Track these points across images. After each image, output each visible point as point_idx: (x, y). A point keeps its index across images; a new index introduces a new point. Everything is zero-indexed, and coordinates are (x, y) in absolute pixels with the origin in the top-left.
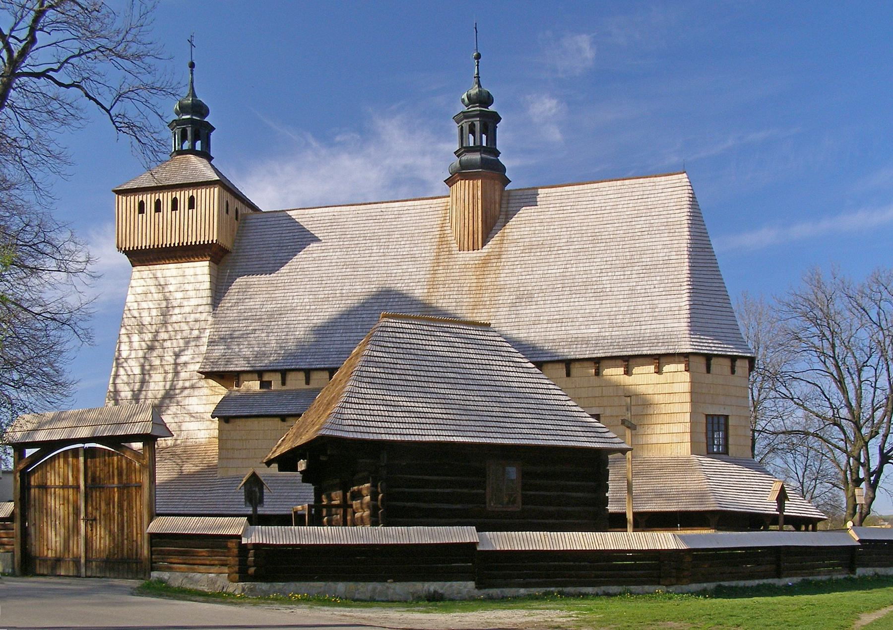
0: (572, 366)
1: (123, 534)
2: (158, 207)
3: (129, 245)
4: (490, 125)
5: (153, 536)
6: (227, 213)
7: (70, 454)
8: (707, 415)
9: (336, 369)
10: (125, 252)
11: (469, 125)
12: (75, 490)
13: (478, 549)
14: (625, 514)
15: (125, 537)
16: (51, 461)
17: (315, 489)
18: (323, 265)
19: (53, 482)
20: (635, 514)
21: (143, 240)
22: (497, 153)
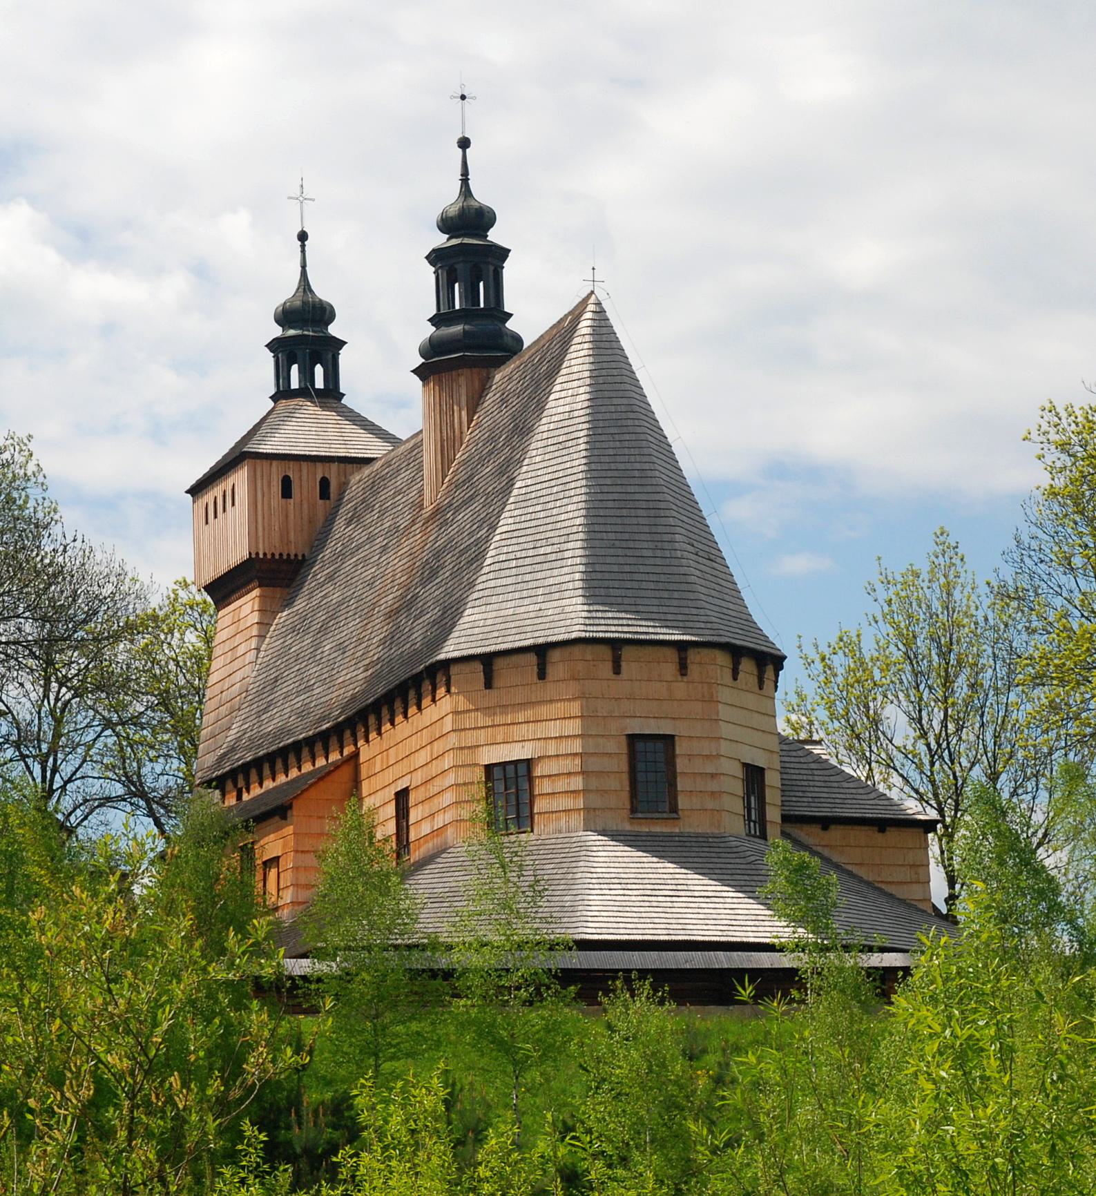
6: (207, 523)
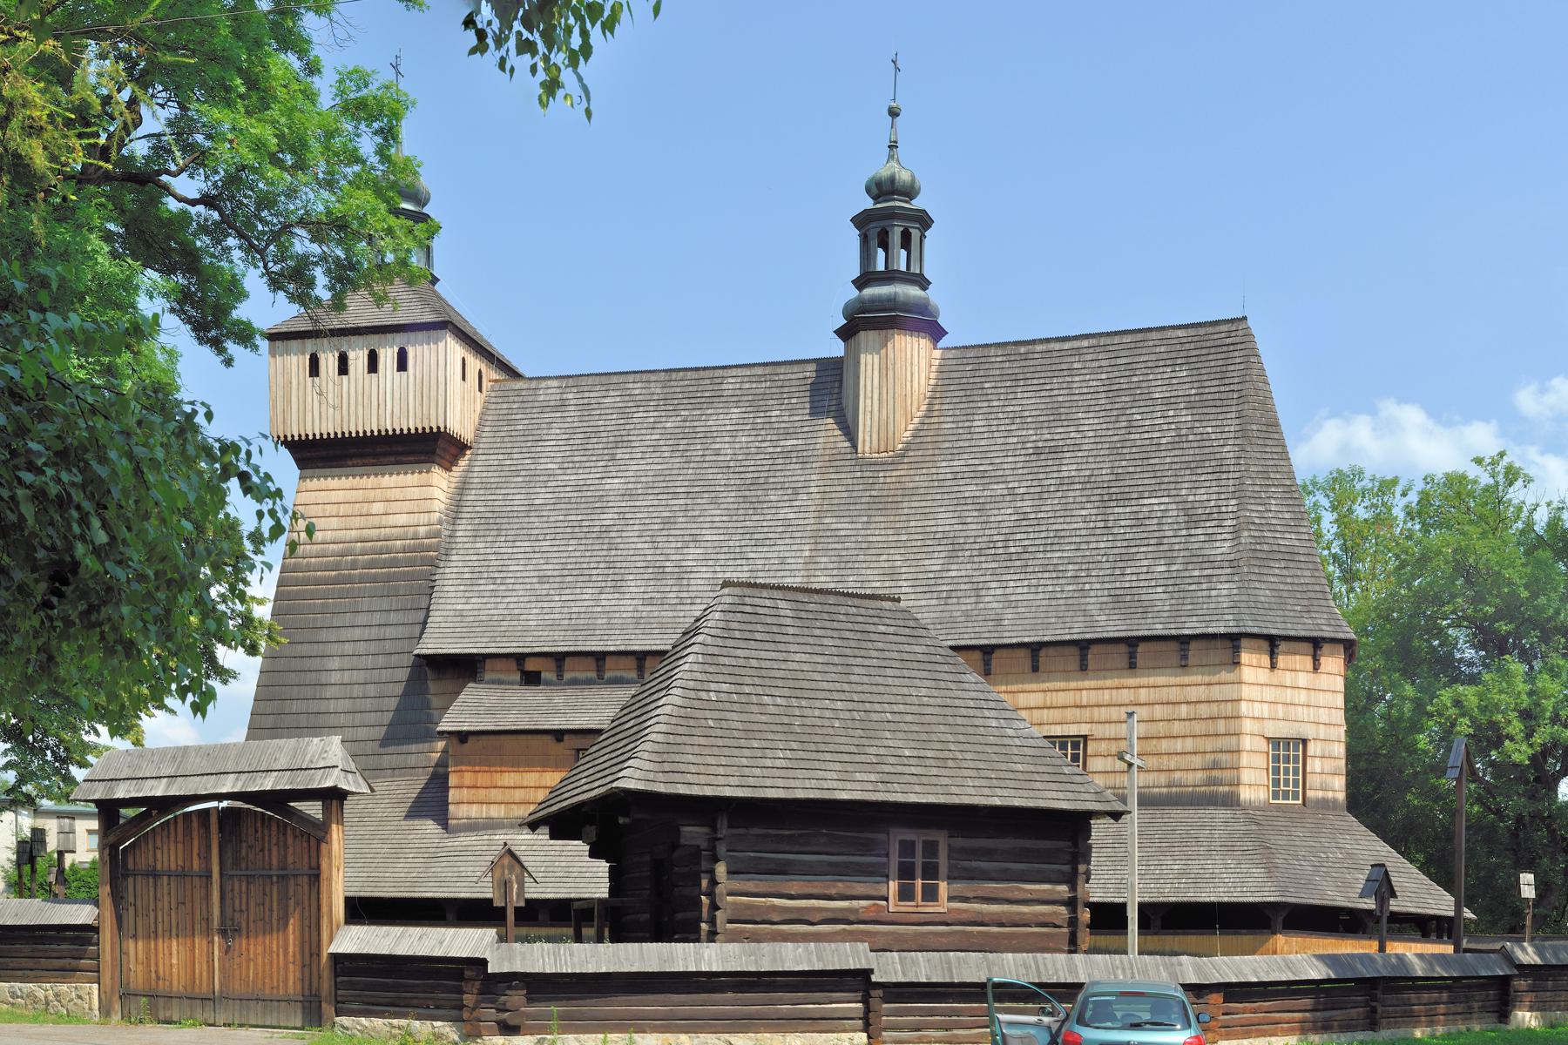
0: (1042, 653)
1: (286, 953)
2: (373, 365)
3: (295, 431)
4: (915, 234)
5: (337, 958)
6: (464, 379)
7: (195, 819)
8: (1275, 742)
9: (1061, 741)
10: (286, 443)
11: (879, 233)
12: (204, 879)
13: (334, 826)
14: (1123, 906)
15: (291, 959)
16: (163, 830)
17: (611, 869)
18: (866, 507)
19: (166, 864)
20: (1144, 908)
21: (322, 423)
22: (923, 283)
